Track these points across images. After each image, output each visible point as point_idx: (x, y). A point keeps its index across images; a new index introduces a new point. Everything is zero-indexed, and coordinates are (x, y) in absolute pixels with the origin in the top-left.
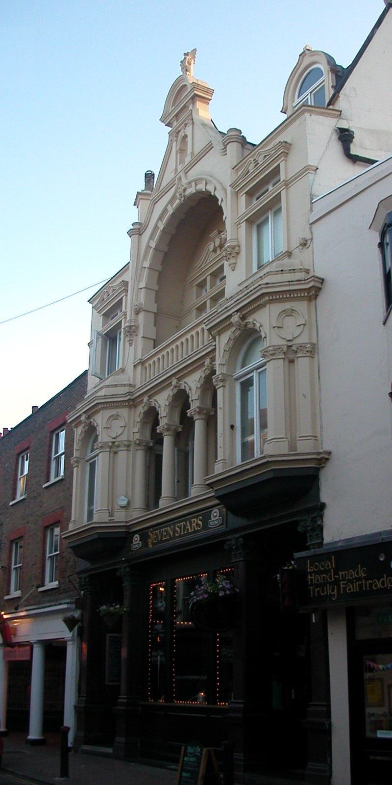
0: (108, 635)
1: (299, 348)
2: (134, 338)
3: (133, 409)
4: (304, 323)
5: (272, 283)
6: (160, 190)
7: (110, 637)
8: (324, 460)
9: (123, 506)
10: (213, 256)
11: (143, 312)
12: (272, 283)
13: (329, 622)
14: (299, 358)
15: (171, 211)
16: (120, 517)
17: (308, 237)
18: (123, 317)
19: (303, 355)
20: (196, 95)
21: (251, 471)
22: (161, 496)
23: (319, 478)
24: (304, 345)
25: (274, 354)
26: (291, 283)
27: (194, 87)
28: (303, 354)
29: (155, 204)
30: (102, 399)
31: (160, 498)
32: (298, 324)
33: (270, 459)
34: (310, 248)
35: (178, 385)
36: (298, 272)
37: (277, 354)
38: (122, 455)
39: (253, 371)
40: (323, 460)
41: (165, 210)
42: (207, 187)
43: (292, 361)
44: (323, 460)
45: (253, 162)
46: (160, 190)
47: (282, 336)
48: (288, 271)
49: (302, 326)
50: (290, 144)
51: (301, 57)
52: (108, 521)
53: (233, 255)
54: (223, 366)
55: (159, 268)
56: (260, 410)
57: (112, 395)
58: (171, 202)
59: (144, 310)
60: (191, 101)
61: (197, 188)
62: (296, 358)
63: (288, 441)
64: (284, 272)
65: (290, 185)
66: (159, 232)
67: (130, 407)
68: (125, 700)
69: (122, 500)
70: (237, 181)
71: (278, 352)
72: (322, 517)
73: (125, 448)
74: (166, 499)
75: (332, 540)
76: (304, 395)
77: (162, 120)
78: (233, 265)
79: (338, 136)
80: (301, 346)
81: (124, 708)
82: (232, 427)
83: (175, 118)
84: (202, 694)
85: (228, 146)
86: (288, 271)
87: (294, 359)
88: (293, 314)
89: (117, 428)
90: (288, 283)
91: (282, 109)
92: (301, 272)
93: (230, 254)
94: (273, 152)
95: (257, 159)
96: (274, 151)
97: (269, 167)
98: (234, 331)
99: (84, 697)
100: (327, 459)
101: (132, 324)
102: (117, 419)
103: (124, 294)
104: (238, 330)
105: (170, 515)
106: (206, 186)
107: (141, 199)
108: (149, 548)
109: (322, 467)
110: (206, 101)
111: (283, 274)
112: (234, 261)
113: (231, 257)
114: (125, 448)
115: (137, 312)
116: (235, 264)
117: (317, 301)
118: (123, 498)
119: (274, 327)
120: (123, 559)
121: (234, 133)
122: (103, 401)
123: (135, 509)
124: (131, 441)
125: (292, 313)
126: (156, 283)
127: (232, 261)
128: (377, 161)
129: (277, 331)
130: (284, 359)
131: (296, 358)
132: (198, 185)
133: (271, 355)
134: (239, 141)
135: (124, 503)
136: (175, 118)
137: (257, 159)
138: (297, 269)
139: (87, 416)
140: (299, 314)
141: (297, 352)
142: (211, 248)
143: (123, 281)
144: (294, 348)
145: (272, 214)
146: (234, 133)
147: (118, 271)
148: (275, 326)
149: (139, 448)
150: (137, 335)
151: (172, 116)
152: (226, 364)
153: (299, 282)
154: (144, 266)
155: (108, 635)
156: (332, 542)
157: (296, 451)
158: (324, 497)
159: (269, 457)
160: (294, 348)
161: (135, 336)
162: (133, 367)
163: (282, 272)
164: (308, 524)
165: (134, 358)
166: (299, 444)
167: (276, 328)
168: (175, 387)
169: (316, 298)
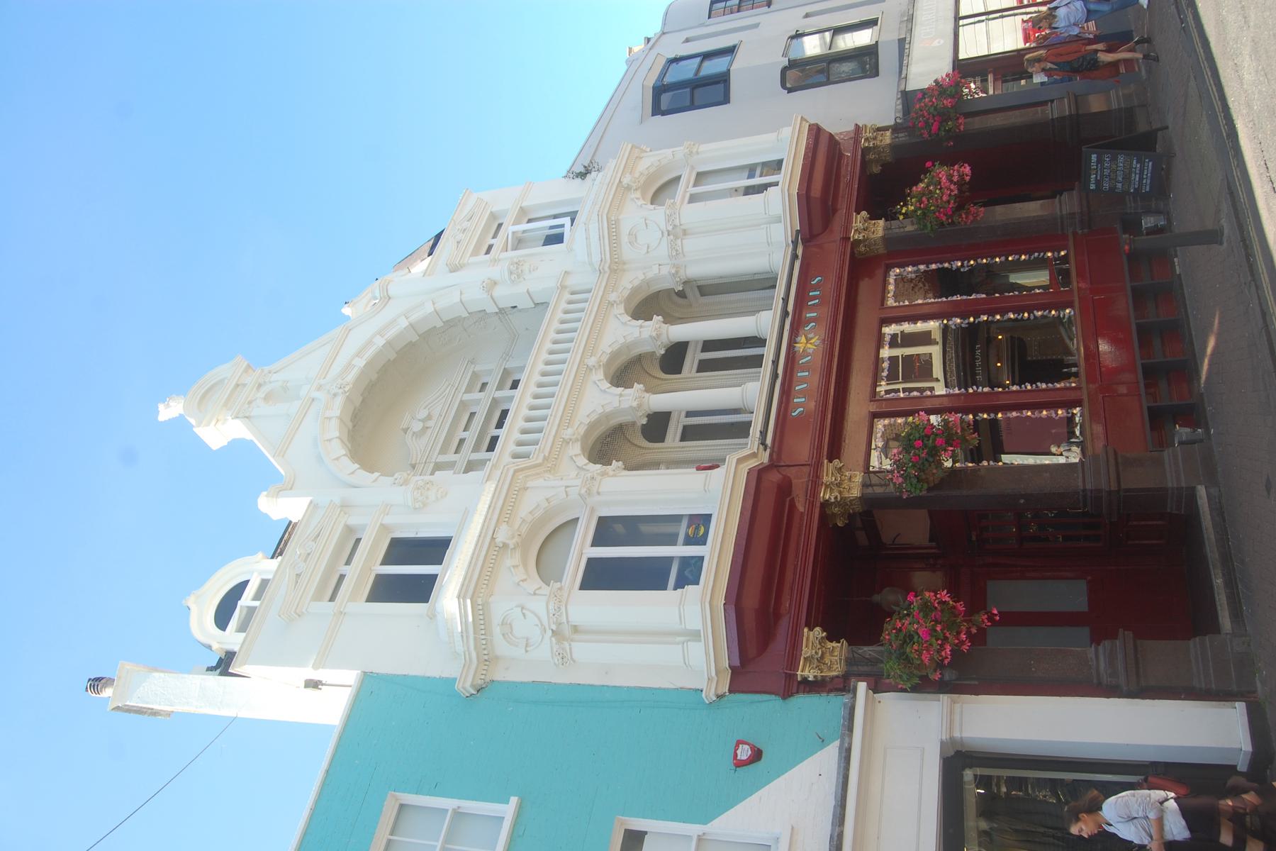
4: (520, 609)
14: (570, 619)
32: (523, 617)
43: (685, 232)
47: (540, 640)
49: (524, 611)
56: (673, 557)
62: (682, 227)
63: (689, 640)
77: (726, 100)
87: (571, 626)
88: (634, 233)
99: (1061, 212)
119: (527, 651)
125: (506, 624)
128: (245, 583)
129: (532, 648)
130: (682, 240)
131: (682, 227)
140: (507, 615)
141: (675, 225)
144: (670, 228)
148: (524, 651)
157: (700, 631)
160: (670, 228)
167: (528, 649)
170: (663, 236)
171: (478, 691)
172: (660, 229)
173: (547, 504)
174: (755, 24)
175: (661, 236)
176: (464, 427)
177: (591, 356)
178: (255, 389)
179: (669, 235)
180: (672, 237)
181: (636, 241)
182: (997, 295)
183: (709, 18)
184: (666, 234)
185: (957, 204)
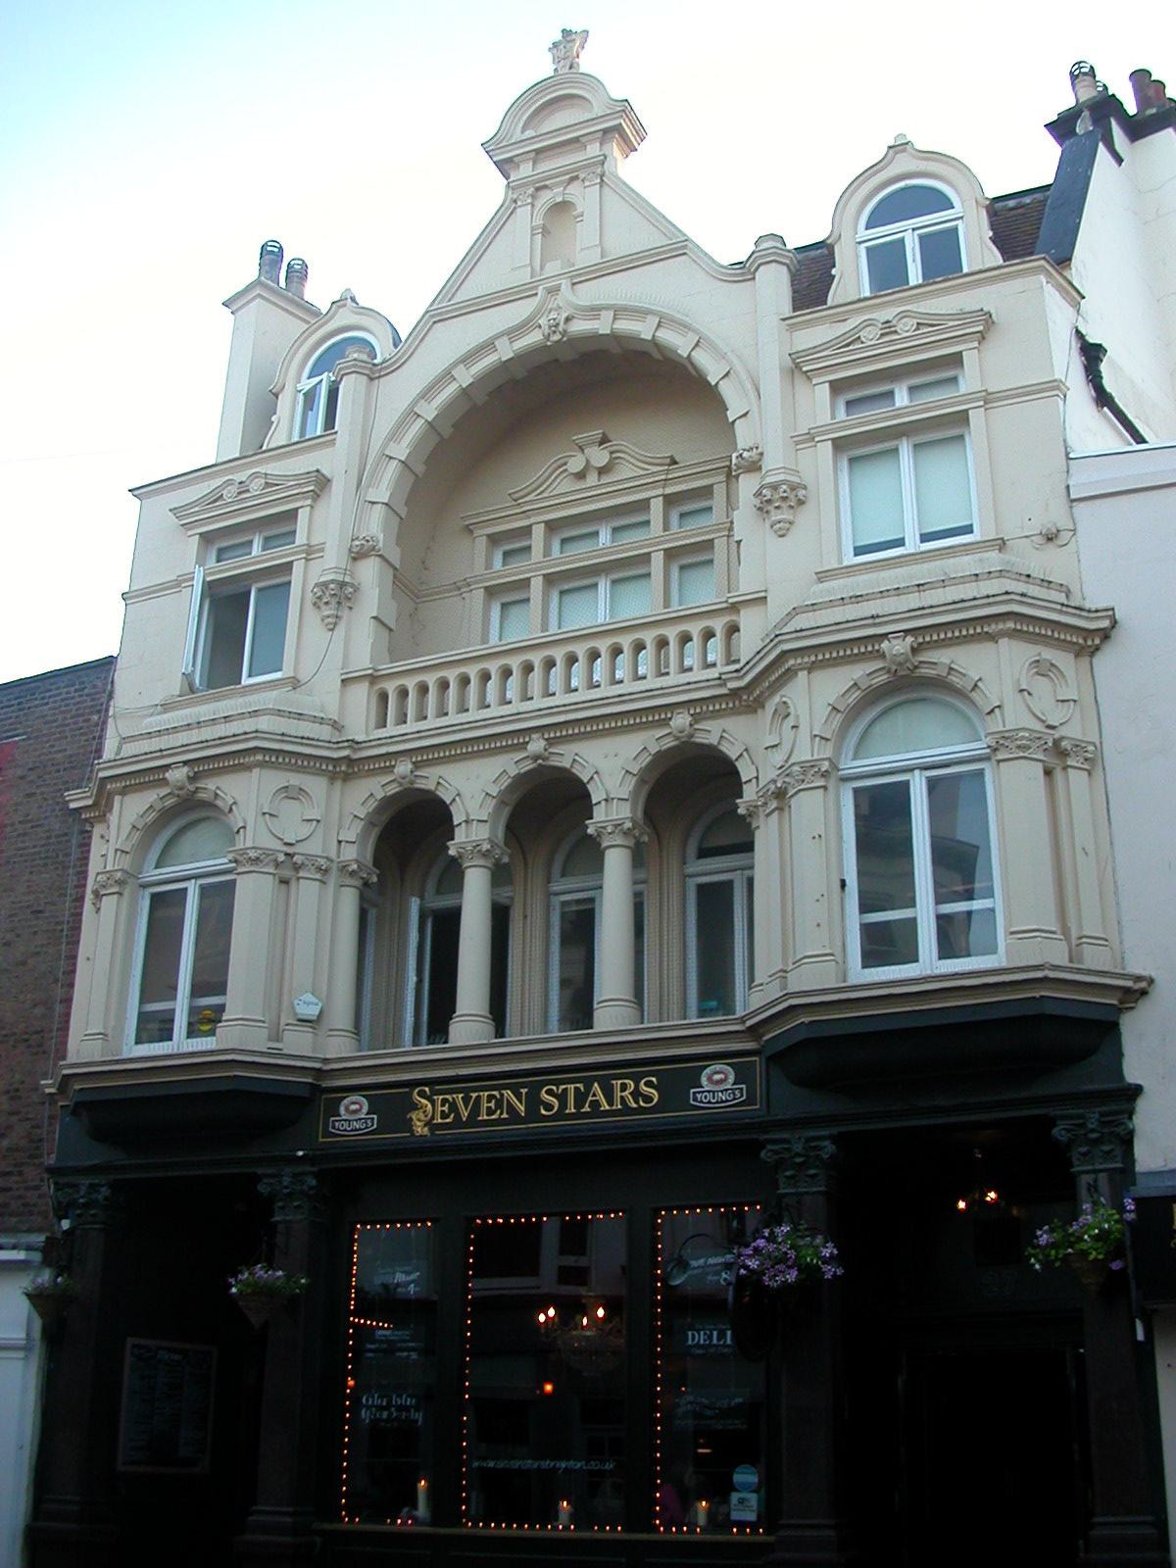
0: (130, 1341)
1: (1001, 742)
2: (345, 613)
3: (338, 784)
5: (1033, 598)
6: (452, 302)
7: (134, 1346)
8: (1138, 995)
9: (305, 1017)
10: (566, 486)
11: (377, 559)
12: (1033, 598)
13: (1156, 1332)
15: (506, 351)
16: (298, 1045)
17: (1064, 523)
18: (304, 555)
19: (1076, 765)
20: (618, 129)
21: (980, 992)
22: (455, 1012)
23: (1119, 1030)
24: (1084, 745)
25: (1026, 748)
26: (1064, 609)
27: (623, 111)
28: (1077, 762)
29: (435, 322)
30: (274, 740)
31: (451, 1019)
33: (1052, 974)
34: (1072, 546)
35: (546, 754)
36: (1056, 590)
37: (1032, 750)
38: (307, 891)
39: (912, 770)
40: (1136, 992)
41: (488, 346)
42: (657, 334)
44: (1136, 992)
45: (880, 326)
46: (452, 302)
48: (997, 574)
50: (993, 323)
51: (891, 151)
52: (265, 1050)
53: (777, 504)
54: (823, 742)
55: (420, 469)
57: (302, 738)
58: (513, 333)
59: (380, 556)
60: (600, 134)
61: (614, 326)
64: (1031, 580)
65: (995, 405)
66: (451, 389)
67: (333, 777)
68: (289, 1519)
69: (308, 1004)
70: (818, 349)
71: (1034, 745)
72: (1131, 1114)
73: (318, 876)
74: (483, 1022)
75: (1166, 1165)
76: (1084, 849)
77: (489, 148)
78: (787, 525)
79: (1079, 345)
80: (1077, 746)
81: (288, 1539)
82: (843, 884)
83: (533, 155)
84: (704, 1503)
85: (757, 274)
86: (1039, 582)
89: (292, 824)
90: (1059, 607)
91: (827, 239)
92: (1060, 591)
93: (784, 499)
94: (951, 324)
95: (894, 322)
96: (956, 323)
97: (906, 355)
98: (871, 673)
100: (1144, 993)
101: (347, 579)
102: (298, 799)
103: (309, 502)
104: (884, 672)
105: (511, 1061)
106: (656, 330)
107: (259, 295)
108: (413, 1135)
109: (1127, 1008)
110: (630, 148)
111: (1028, 583)
112: (791, 518)
113: (784, 505)
114: (318, 876)
115: (358, 556)
116: (788, 529)
117: (1094, 660)
118: (309, 997)
119: (264, 814)
120: (300, 1153)
121: (771, 244)
122: (276, 746)
123: (331, 1030)
124: (332, 861)
126: (404, 502)
127: (786, 515)
130: (274, 875)
131: (294, 879)
132: (662, 329)
133: (1019, 747)
134: (792, 267)
135: (312, 1012)
136: (533, 155)
137: (894, 322)
138: (1056, 584)
139: (191, 774)
142: (576, 464)
143: (318, 471)
145: (910, 448)
146: (771, 244)
147: (1154, 492)
149: (349, 881)
150: (351, 608)
151: (528, 149)
152: (833, 740)
153: (1078, 612)
154: (387, 453)
155: (130, 1341)
156: (1162, 1169)
158: (1133, 1071)
159: (1050, 970)
161: (347, 610)
162: (339, 682)
163: (1027, 579)
164: (1091, 1126)
165: (343, 663)
166: (1087, 950)
167: (818, 739)
168: (536, 758)
169: (1092, 654)
170: (286, 844)
171: (976, 685)
172: (297, 842)
173: (970, 689)
174: (1141, 436)
175: (286, 840)
176: (556, 624)
177: (546, 740)
178: (568, 177)
179: (287, 854)
180: (281, 858)
181: (1037, 673)
182: (300, 1153)
183: (494, 782)
184: (290, 850)
185: (239, 1268)
